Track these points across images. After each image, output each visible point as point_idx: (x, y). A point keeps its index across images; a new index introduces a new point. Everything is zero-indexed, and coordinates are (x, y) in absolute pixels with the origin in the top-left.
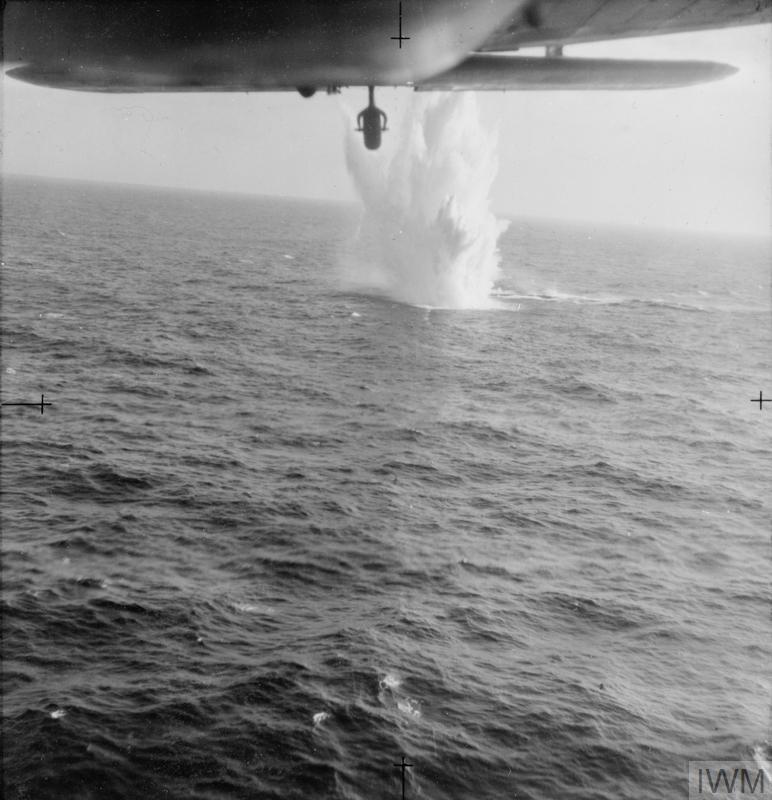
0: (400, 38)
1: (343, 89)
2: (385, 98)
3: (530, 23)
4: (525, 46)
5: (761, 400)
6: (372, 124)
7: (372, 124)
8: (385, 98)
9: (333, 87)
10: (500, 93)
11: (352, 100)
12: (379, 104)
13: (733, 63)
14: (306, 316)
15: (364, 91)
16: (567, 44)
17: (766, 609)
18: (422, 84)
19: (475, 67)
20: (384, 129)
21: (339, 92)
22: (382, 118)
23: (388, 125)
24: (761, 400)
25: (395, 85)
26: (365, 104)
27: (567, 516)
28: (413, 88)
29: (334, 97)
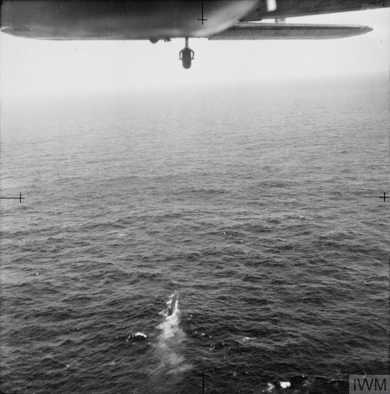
0: (203, 20)
1: (172, 39)
2: (193, 43)
3: (260, 11)
4: (265, 19)
5: (21, 198)
6: (187, 57)
7: (187, 57)
8: (193, 43)
9: (168, 38)
10: (253, 41)
11: (178, 44)
12: (190, 47)
13: (370, 26)
14: (289, 217)
15: (184, 39)
16: (273, 24)
17: (4, 194)
18: (212, 37)
19: (232, 32)
20: (193, 59)
21: (170, 40)
22: (192, 53)
23: (194, 57)
24: (21, 198)
25: (199, 37)
26: (183, 47)
27: (107, 321)
28: (208, 39)
29: (168, 43)
